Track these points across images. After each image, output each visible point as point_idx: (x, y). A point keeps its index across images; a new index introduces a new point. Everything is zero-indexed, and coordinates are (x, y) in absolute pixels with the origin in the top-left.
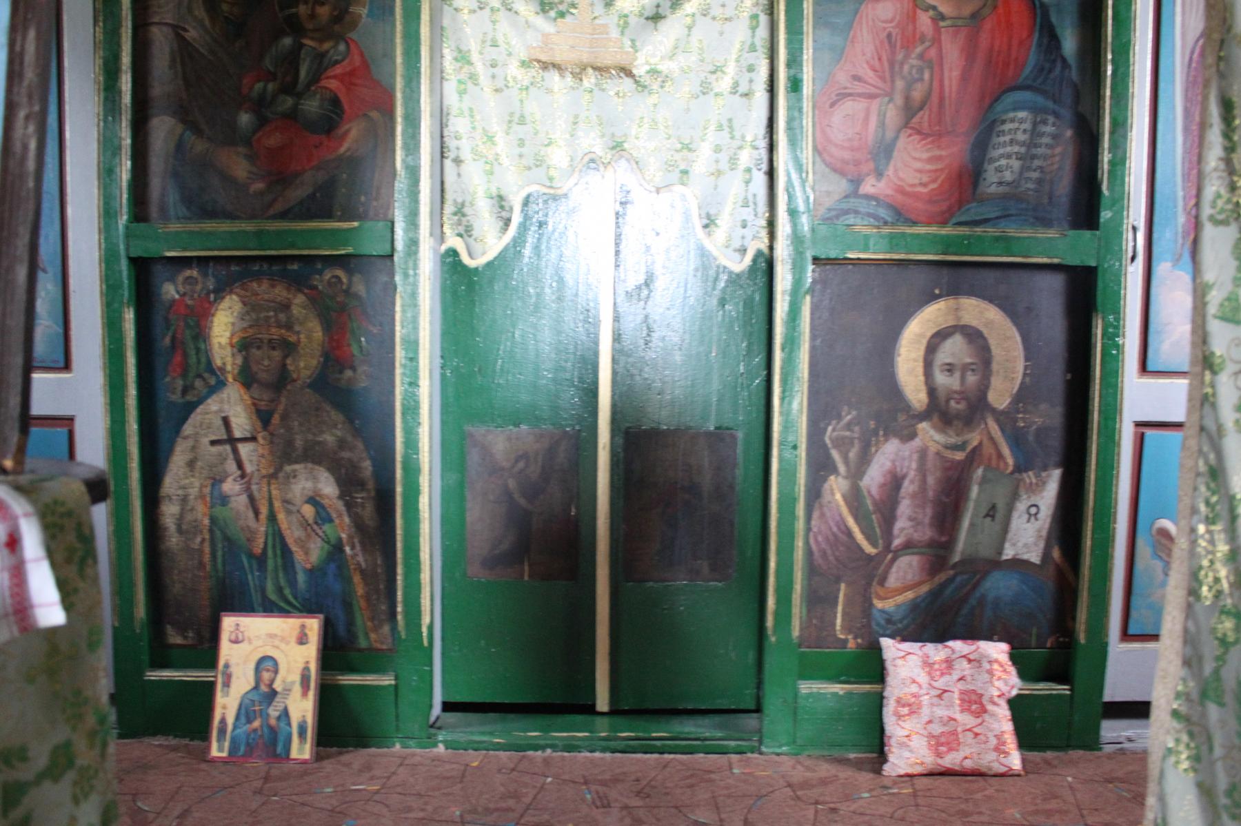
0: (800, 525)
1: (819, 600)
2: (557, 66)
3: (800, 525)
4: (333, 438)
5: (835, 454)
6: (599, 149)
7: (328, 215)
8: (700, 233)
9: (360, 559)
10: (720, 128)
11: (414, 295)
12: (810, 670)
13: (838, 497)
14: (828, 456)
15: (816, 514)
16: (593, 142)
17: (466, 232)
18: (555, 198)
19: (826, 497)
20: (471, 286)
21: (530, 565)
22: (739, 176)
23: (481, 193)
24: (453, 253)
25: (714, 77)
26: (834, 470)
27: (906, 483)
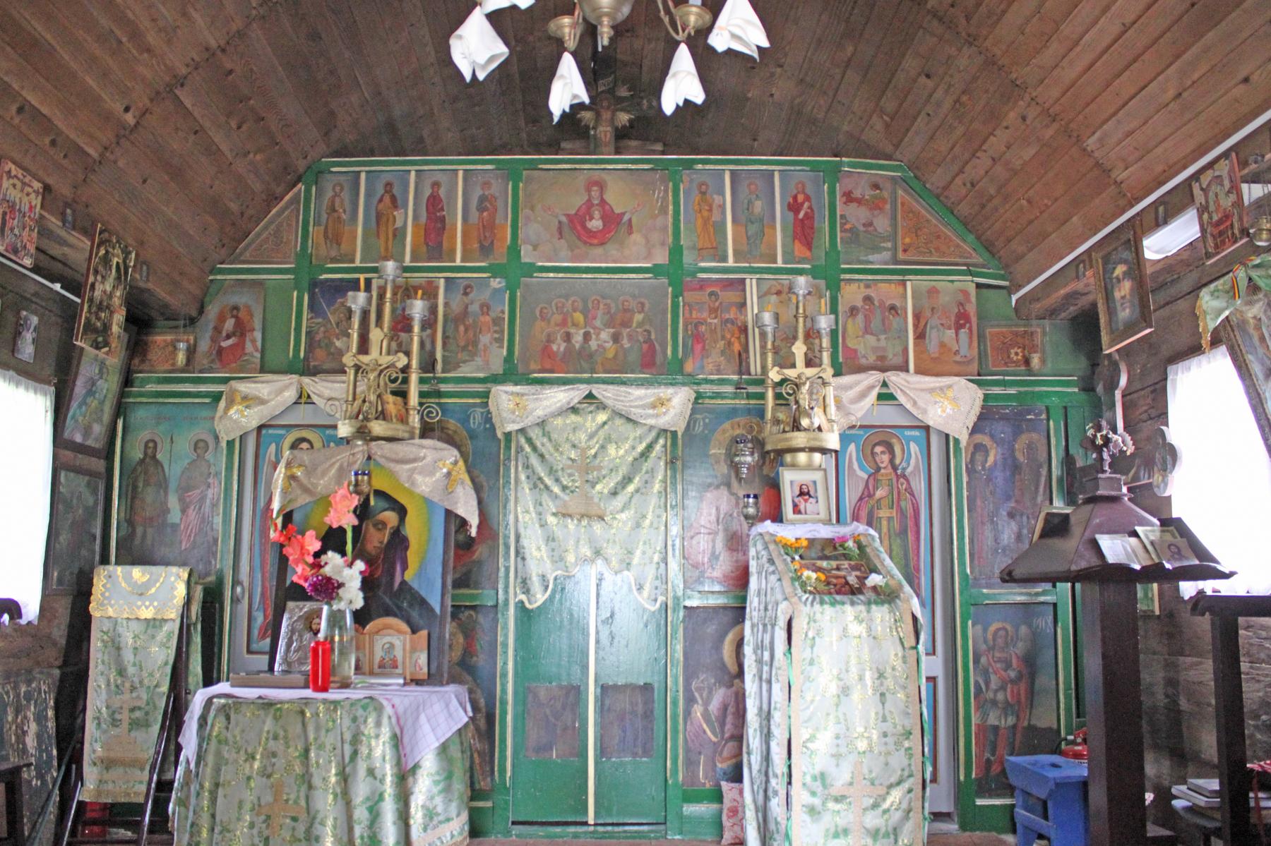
0: (681, 727)
1: (691, 763)
2: (570, 516)
3: (681, 727)
5: (697, 695)
6: (589, 554)
7: (467, 586)
8: (635, 592)
9: (478, 745)
10: (645, 543)
11: (506, 624)
12: (689, 798)
13: (699, 714)
14: (693, 696)
15: (689, 723)
16: (586, 551)
17: (527, 591)
18: (569, 577)
19: (693, 715)
20: (529, 618)
22: (654, 566)
23: (534, 574)
24: (522, 602)
25: (177, 24)
26: (697, 702)
27: (730, 708)
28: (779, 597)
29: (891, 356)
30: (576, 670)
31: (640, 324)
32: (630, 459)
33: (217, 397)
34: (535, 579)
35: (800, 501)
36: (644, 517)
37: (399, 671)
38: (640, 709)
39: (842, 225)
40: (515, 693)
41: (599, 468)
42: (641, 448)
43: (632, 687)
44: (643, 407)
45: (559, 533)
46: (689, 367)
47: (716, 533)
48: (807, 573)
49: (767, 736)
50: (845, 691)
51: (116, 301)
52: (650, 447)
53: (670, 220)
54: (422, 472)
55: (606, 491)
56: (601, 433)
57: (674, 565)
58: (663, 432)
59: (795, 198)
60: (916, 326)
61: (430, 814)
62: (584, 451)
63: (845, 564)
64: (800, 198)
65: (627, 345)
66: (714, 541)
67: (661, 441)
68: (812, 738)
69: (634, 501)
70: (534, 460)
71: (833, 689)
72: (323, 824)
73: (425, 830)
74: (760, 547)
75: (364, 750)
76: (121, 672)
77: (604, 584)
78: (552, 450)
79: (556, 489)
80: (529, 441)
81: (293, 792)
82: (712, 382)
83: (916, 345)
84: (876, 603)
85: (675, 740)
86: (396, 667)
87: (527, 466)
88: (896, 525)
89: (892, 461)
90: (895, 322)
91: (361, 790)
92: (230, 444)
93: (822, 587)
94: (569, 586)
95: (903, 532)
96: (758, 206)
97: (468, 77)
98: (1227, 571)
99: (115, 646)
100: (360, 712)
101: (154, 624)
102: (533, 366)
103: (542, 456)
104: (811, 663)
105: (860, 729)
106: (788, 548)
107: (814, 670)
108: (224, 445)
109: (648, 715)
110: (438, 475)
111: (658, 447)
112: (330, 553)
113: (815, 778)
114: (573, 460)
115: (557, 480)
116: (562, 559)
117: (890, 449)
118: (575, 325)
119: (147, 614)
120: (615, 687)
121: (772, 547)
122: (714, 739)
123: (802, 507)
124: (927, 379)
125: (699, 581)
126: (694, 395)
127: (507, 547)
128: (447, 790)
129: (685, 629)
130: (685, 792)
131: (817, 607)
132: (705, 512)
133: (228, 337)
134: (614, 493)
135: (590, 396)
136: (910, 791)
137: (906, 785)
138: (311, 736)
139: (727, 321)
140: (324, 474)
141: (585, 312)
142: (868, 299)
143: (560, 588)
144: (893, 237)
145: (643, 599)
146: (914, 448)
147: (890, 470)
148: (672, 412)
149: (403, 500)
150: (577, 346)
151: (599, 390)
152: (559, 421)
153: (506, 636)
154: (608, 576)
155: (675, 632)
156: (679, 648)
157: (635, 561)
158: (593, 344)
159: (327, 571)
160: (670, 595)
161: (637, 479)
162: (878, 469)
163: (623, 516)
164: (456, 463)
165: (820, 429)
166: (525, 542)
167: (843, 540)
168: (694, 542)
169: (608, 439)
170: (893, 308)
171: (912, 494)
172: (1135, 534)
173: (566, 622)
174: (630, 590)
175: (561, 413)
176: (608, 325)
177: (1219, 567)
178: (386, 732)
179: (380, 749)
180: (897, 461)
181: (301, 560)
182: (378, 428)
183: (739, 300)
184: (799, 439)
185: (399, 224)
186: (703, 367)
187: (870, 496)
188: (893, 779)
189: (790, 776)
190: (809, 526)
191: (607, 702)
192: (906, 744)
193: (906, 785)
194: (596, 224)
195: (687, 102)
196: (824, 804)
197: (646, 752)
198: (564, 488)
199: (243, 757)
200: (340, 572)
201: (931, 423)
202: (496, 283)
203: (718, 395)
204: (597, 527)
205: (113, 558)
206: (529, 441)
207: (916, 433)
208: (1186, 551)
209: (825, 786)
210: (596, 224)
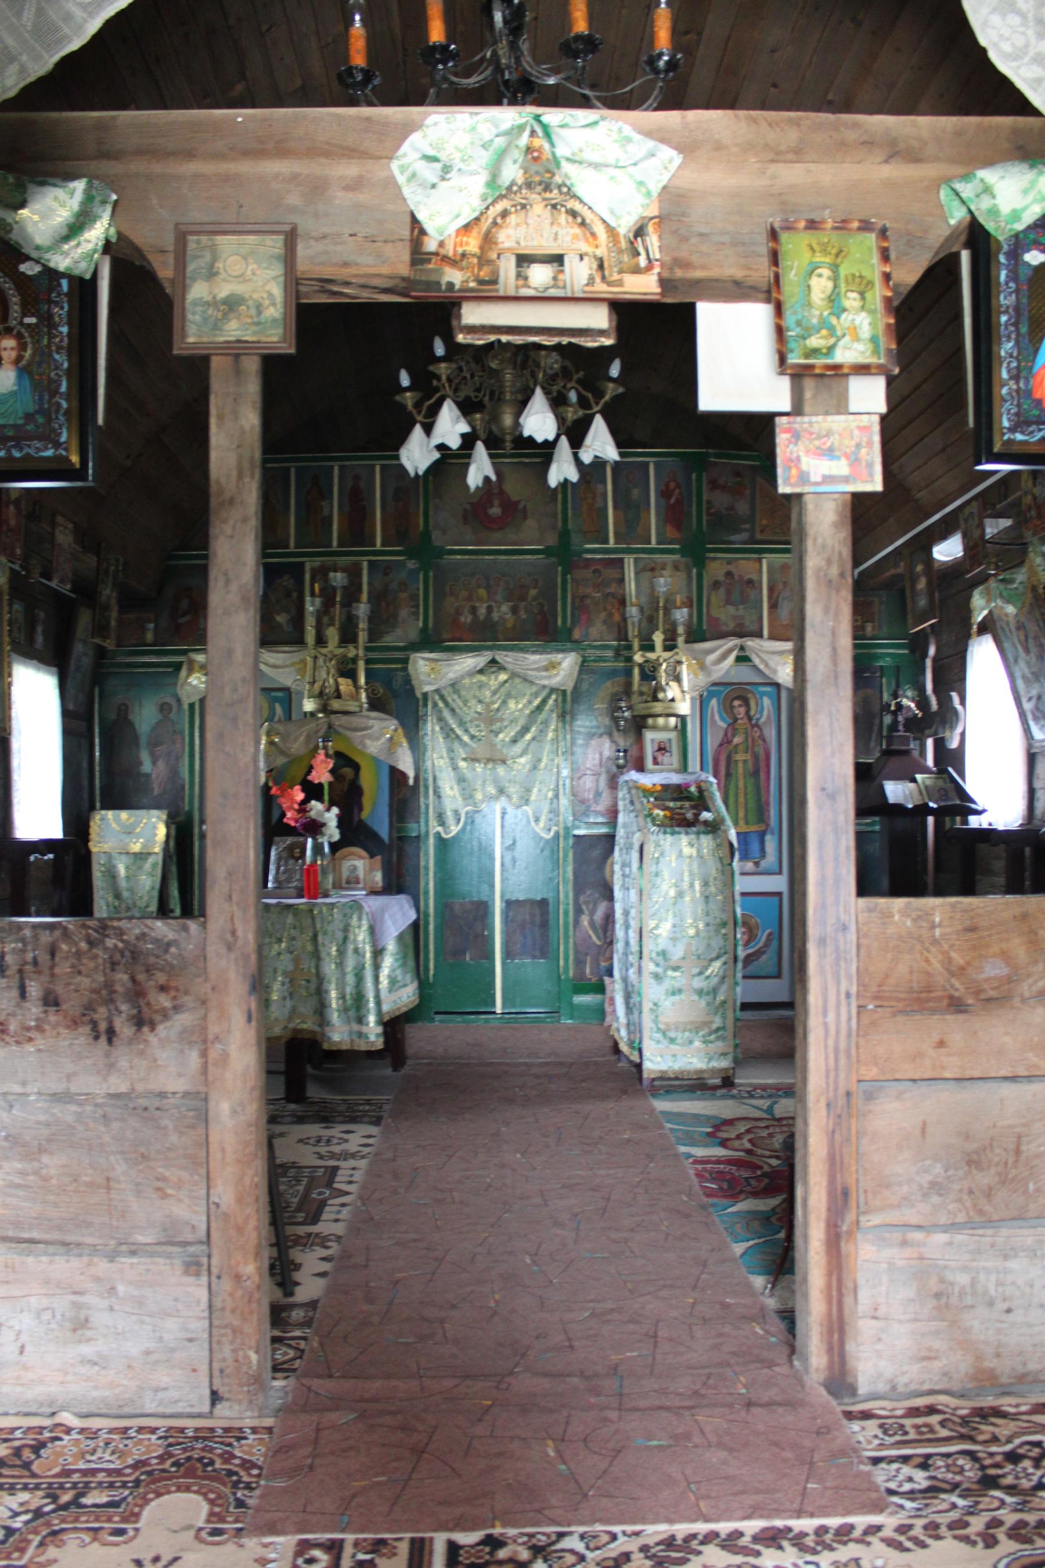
0: (571, 933)
1: (579, 963)
2: (478, 760)
3: (571, 933)
4: (53, 828)
6: (494, 792)
8: (533, 824)
16: (492, 790)
21: (980, 463)
24: (438, 833)
28: (635, 828)
29: (747, 623)
30: (485, 887)
31: (535, 598)
32: (527, 712)
33: (178, 666)
34: (449, 813)
35: (658, 754)
36: (540, 760)
37: (361, 886)
38: (538, 919)
39: (708, 509)
40: (436, 907)
41: (501, 720)
42: (536, 702)
43: (531, 902)
44: (538, 669)
45: (468, 775)
46: (577, 634)
47: (599, 774)
48: (657, 811)
49: (627, 927)
50: (680, 895)
51: (113, 601)
52: (544, 702)
53: (559, 507)
54: (370, 737)
55: (507, 739)
56: (503, 690)
57: (564, 801)
58: (553, 690)
59: (667, 485)
60: (770, 597)
61: (393, 981)
62: (488, 705)
63: (687, 804)
64: (672, 485)
65: (524, 617)
66: (597, 781)
67: (554, 697)
68: (657, 927)
69: (531, 747)
70: (446, 714)
71: (672, 893)
72: (329, 982)
73: (390, 991)
74: (625, 791)
75: (352, 937)
76: (118, 896)
77: (507, 817)
78: (461, 704)
79: (466, 738)
80: (443, 698)
81: (308, 964)
82: (596, 647)
83: (770, 614)
84: (705, 833)
85: (566, 943)
86: (358, 883)
87: (441, 719)
88: (750, 765)
89: (748, 712)
90: (752, 594)
91: (350, 963)
92: (192, 706)
93: (667, 821)
94: (478, 818)
95: (756, 773)
96: (636, 493)
97: (412, 474)
98: (980, 808)
99: (111, 875)
100: (348, 911)
101: (141, 857)
102: (445, 636)
103: (453, 710)
104: (657, 875)
105: (690, 921)
106: (646, 792)
107: (659, 880)
108: (186, 707)
109: (544, 925)
110: (383, 740)
111: (551, 702)
112: (313, 802)
113: (658, 954)
114: (479, 713)
115: (466, 731)
116: (471, 797)
117: (746, 702)
118: (480, 599)
119: (136, 847)
120: (518, 902)
121: (634, 791)
122: (598, 943)
123: (660, 759)
124: (778, 643)
125: (586, 813)
126: (580, 659)
127: (427, 788)
128: (404, 965)
129: (575, 854)
130: (574, 985)
131: (661, 836)
132: (590, 756)
133: (184, 614)
134: (514, 741)
135: (493, 661)
136: (725, 963)
137: (723, 959)
138: (318, 926)
139: (608, 594)
140: (296, 740)
141: (488, 588)
142: (729, 574)
143: (471, 820)
144: (751, 519)
145: (540, 829)
146: (766, 702)
147: (746, 721)
148: (562, 673)
149: (357, 759)
150: (482, 618)
151: (501, 657)
152: (467, 681)
153: (427, 861)
154: (510, 810)
155: (566, 856)
156: (570, 869)
157: (533, 798)
158: (495, 616)
159: (313, 814)
160: (562, 826)
161: (533, 729)
162: (736, 720)
163: (523, 760)
164: (396, 730)
165: (673, 700)
166: (440, 783)
167: (688, 786)
168: (582, 781)
169: (509, 696)
170: (750, 582)
171: (764, 741)
172: (914, 780)
173: (476, 849)
174: (529, 822)
175: (471, 674)
176: (508, 599)
177: (973, 806)
178: (365, 923)
179: (362, 936)
180: (752, 713)
181: (291, 808)
182: (336, 705)
183: (619, 576)
184: (658, 708)
185: (326, 512)
186: (587, 635)
187: (729, 742)
188: (713, 955)
189: (641, 952)
190: (664, 775)
191: (511, 914)
192: (723, 931)
193: (723, 959)
194: (495, 511)
195: (566, 480)
196: (665, 971)
197: (544, 954)
198: (472, 737)
199: (274, 940)
200: (322, 815)
201: (780, 681)
202: (412, 564)
203: (601, 659)
204: (501, 770)
205: (98, 805)
206: (443, 698)
207: (768, 689)
208: (952, 794)
209: (666, 959)
210: (495, 511)
